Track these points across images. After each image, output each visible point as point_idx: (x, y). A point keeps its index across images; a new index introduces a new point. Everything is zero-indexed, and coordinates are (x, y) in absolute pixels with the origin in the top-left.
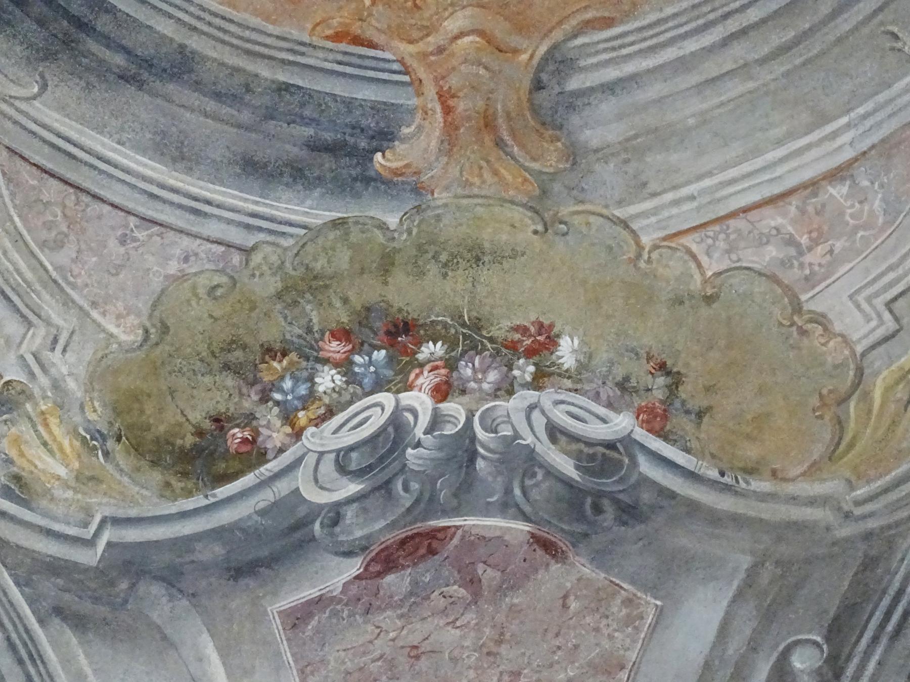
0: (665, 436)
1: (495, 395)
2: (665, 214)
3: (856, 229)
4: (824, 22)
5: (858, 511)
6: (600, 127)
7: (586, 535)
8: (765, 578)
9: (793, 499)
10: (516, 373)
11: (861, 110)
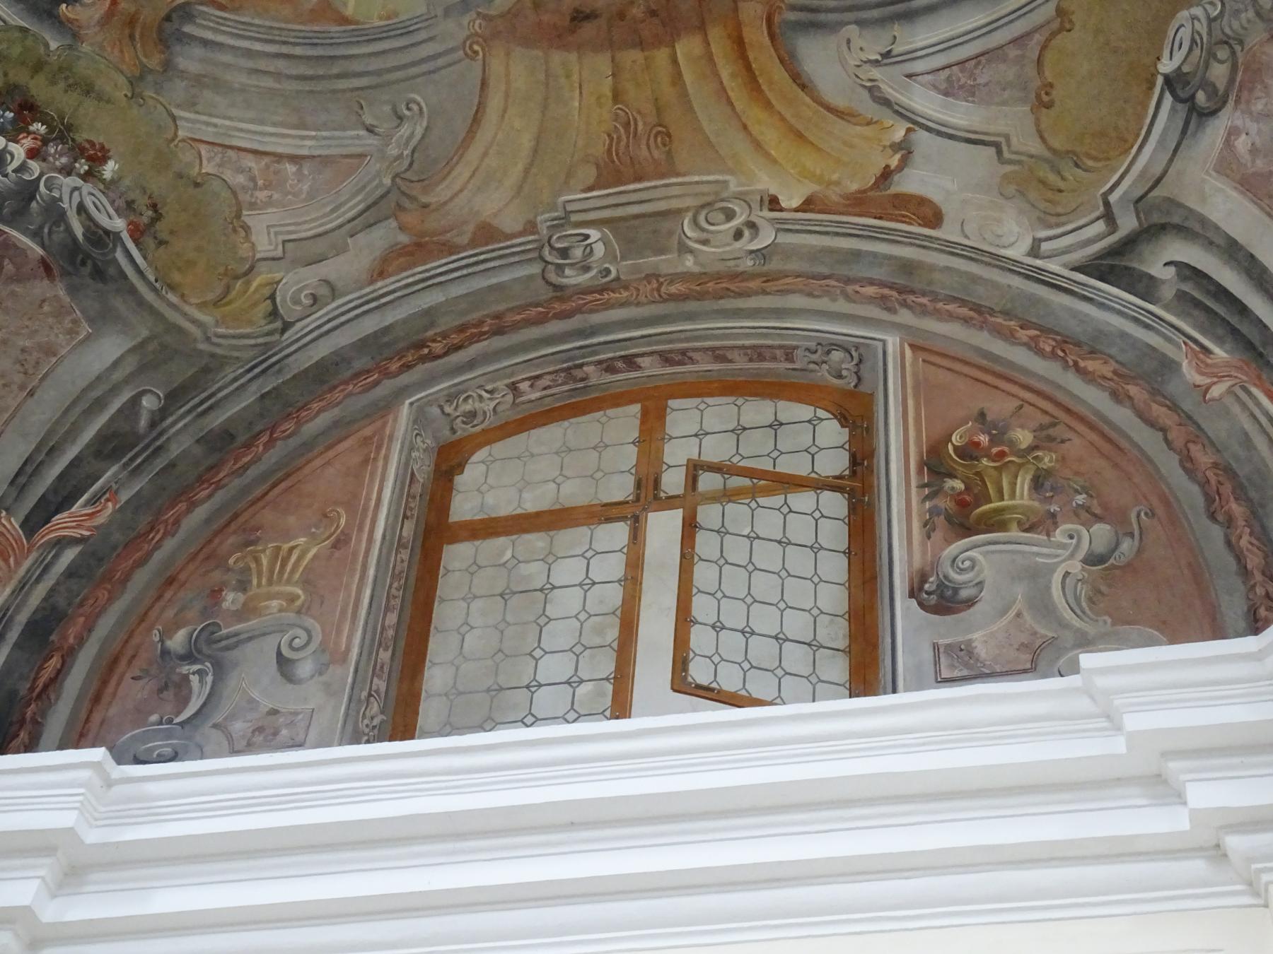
0: (137, 243)
1: (60, 171)
2: (198, 126)
3: (289, 193)
4: (330, 77)
5: (215, 340)
6: (189, 60)
7: (69, 274)
8: (151, 347)
9: (185, 315)
10: (77, 165)
11: (324, 134)
